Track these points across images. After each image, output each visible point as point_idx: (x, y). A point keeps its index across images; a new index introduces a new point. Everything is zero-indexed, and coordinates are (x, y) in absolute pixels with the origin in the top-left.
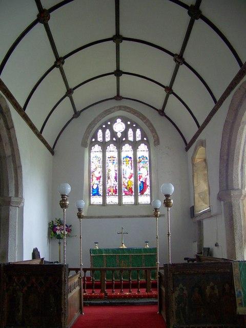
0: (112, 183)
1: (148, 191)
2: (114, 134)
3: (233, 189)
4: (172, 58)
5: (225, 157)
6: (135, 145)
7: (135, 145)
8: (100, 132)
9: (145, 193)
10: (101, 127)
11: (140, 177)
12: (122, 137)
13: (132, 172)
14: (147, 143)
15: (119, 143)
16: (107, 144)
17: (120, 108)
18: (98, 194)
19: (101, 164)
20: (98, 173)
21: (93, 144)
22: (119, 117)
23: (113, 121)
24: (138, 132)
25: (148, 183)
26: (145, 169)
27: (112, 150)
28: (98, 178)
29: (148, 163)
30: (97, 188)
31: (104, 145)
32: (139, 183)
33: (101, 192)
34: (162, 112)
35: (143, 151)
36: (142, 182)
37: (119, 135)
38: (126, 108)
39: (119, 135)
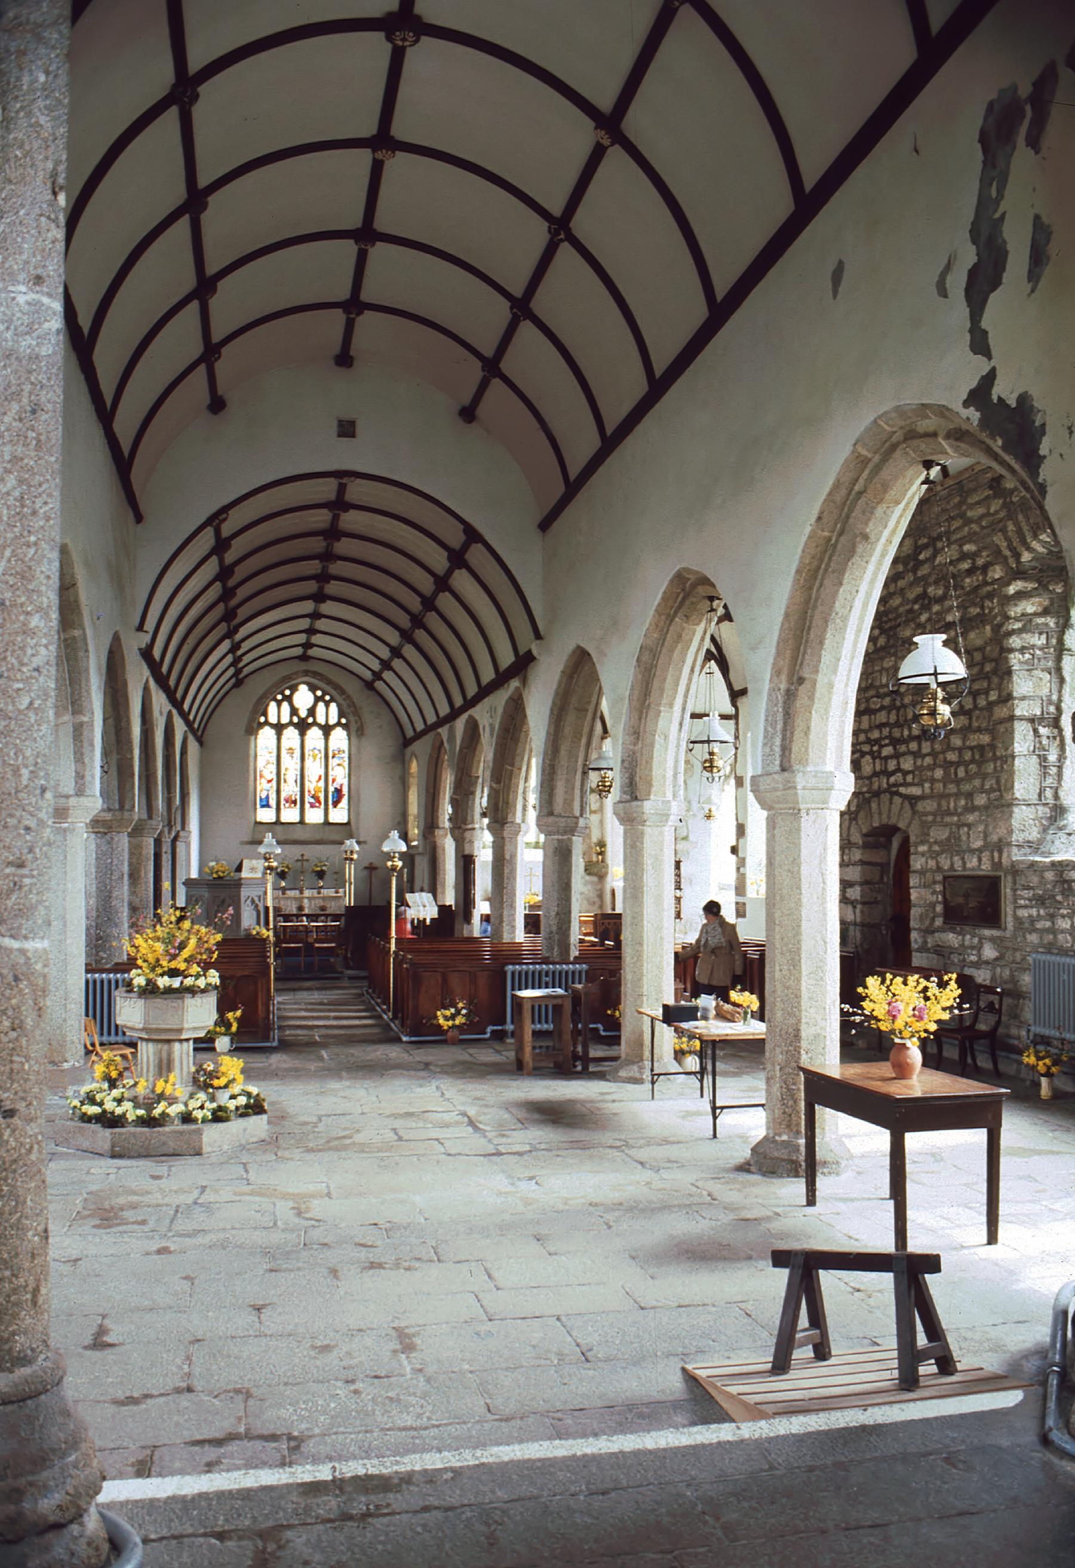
0: (290, 789)
1: (344, 802)
2: (294, 711)
3: (438, 828)
4: (388, 649)
5: (432, 791)
6: (327, 730)
7: (327, 730)
8: (273, 706)
9: (340, 805)
10: (275, 700)
11: (334, 781)
12: (308, 717)
13: (322, 772)
14: (345, 727)
15: (303, 727)
16: (285, 726)
17: (306, 673)
18: (268, 806)
19: (274, 760)
20: (270, 772)
21: (261, 725)
22: (304, 683)
23: (294, 689)
24: (333, 707)
25: (345, 790)
26: (341, 768)
27: (291, 735)
28: (270, 781)
29: (346, 759)
30: (267, 797)
31: (279, 728)
32: (331, 789)
33: (273, 802)
34: (369, 685)
35: (339, 738)
36: (336, 789)
37: (303, 714)
38: (315, 674)
39: (303, 714)
